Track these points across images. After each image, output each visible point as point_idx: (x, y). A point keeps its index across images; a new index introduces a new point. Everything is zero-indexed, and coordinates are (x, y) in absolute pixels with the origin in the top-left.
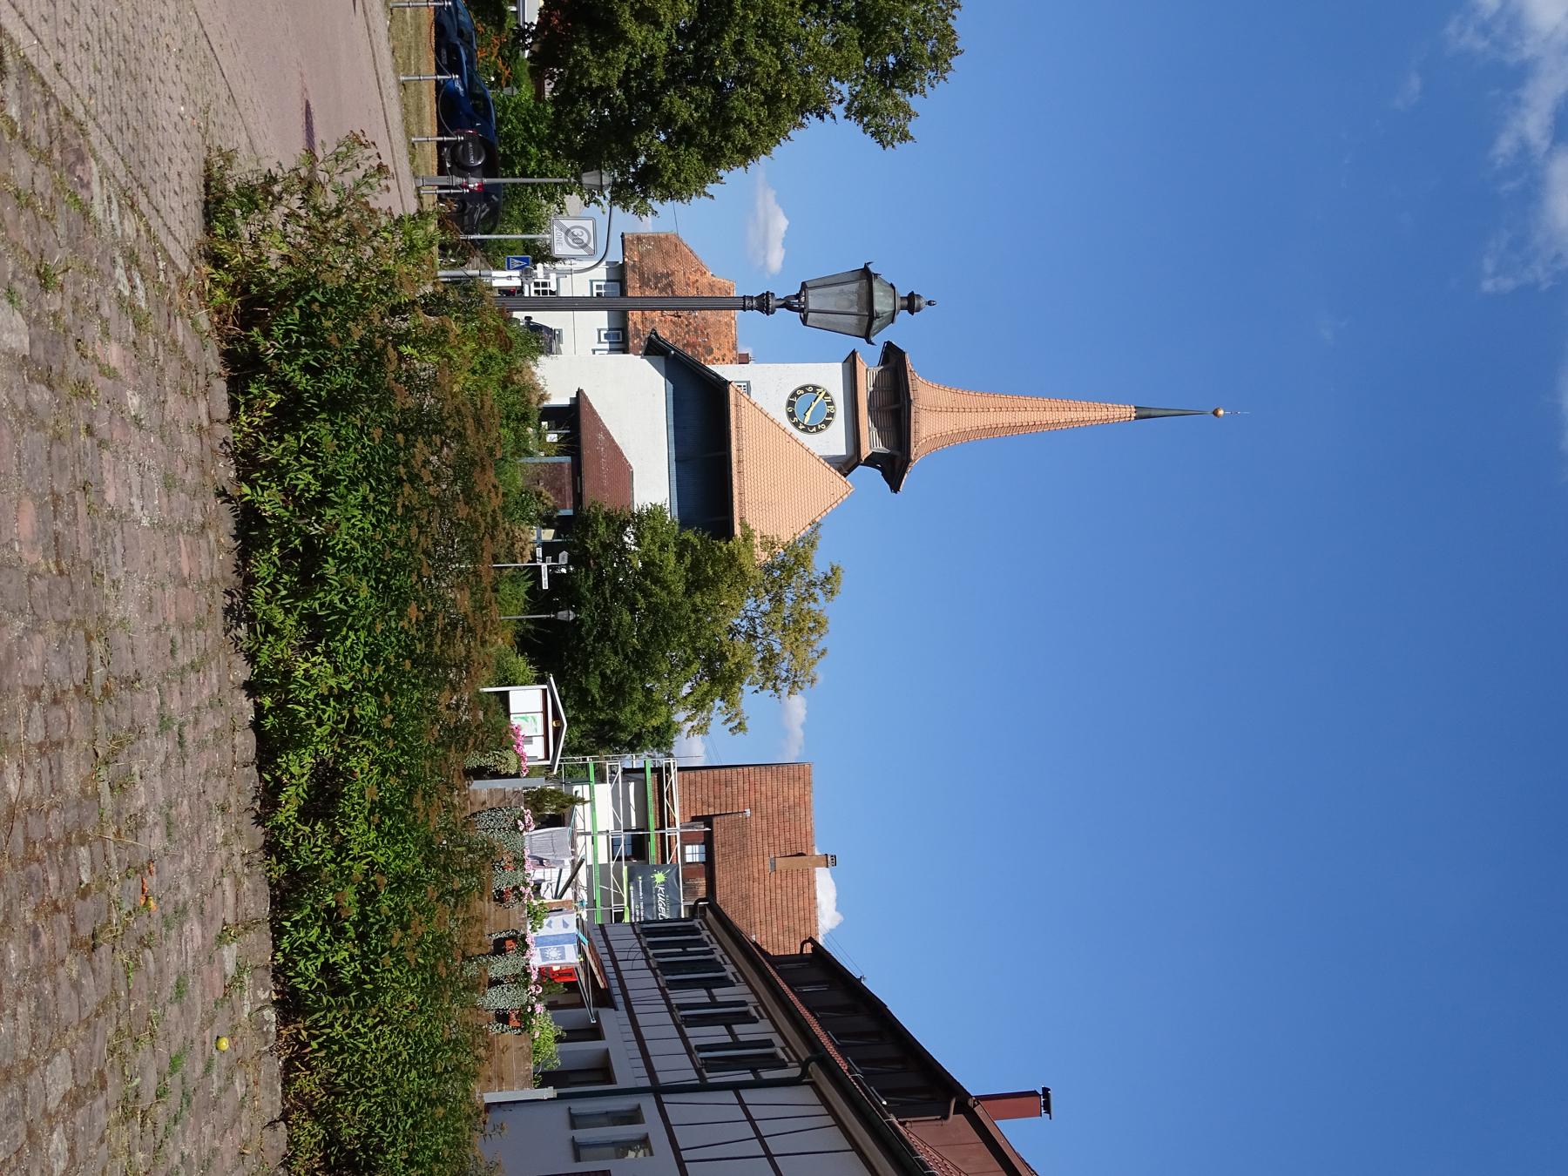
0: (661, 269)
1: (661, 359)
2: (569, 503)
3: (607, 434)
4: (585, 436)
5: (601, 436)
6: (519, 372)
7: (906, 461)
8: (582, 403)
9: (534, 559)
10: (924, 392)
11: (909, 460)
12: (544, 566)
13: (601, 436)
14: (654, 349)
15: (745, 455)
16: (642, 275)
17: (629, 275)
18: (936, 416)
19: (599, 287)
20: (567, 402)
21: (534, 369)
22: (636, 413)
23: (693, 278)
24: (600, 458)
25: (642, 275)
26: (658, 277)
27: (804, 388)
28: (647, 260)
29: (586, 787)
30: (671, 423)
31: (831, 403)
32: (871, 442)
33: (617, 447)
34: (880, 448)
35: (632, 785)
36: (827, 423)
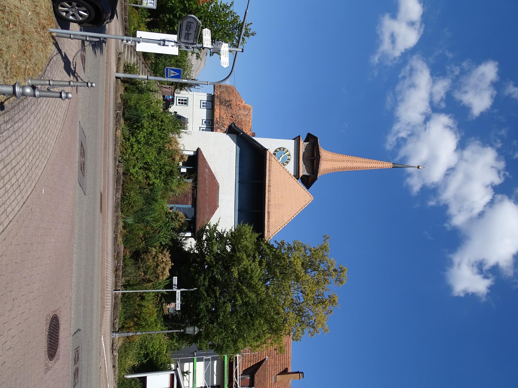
0: (227, 99)
1: (235, 136)
2: (190, 202)
3: (209, 169)
4: (200, 171)
5: (207, 170)
6: (170, 142)
7: (315, 179)
8: (200, 155)
9: (170, 285)
10: (324, 154)
11: (316, 179)
12: (178, 292)
13: (207, 170)
14: (233, 131)
15: (272, 184)
16: (220, 100)
17: (216, 99)
18: (329, 162)
19: (203, 103)
20: (192, 153)
21: (179, 140)
22: (222, 157)
23: (238, 103)
24: (205, 180)
25: (220, 100)
26: (226, 102)
27: (280, 149)
28: (222, 95)
29: (192, 364)
30: (238, 165)
31: (289, 155)
32: (303, 171)
33: (213, 175)
34: (306, 173)
35: (215, 362)
36: (287, 162)
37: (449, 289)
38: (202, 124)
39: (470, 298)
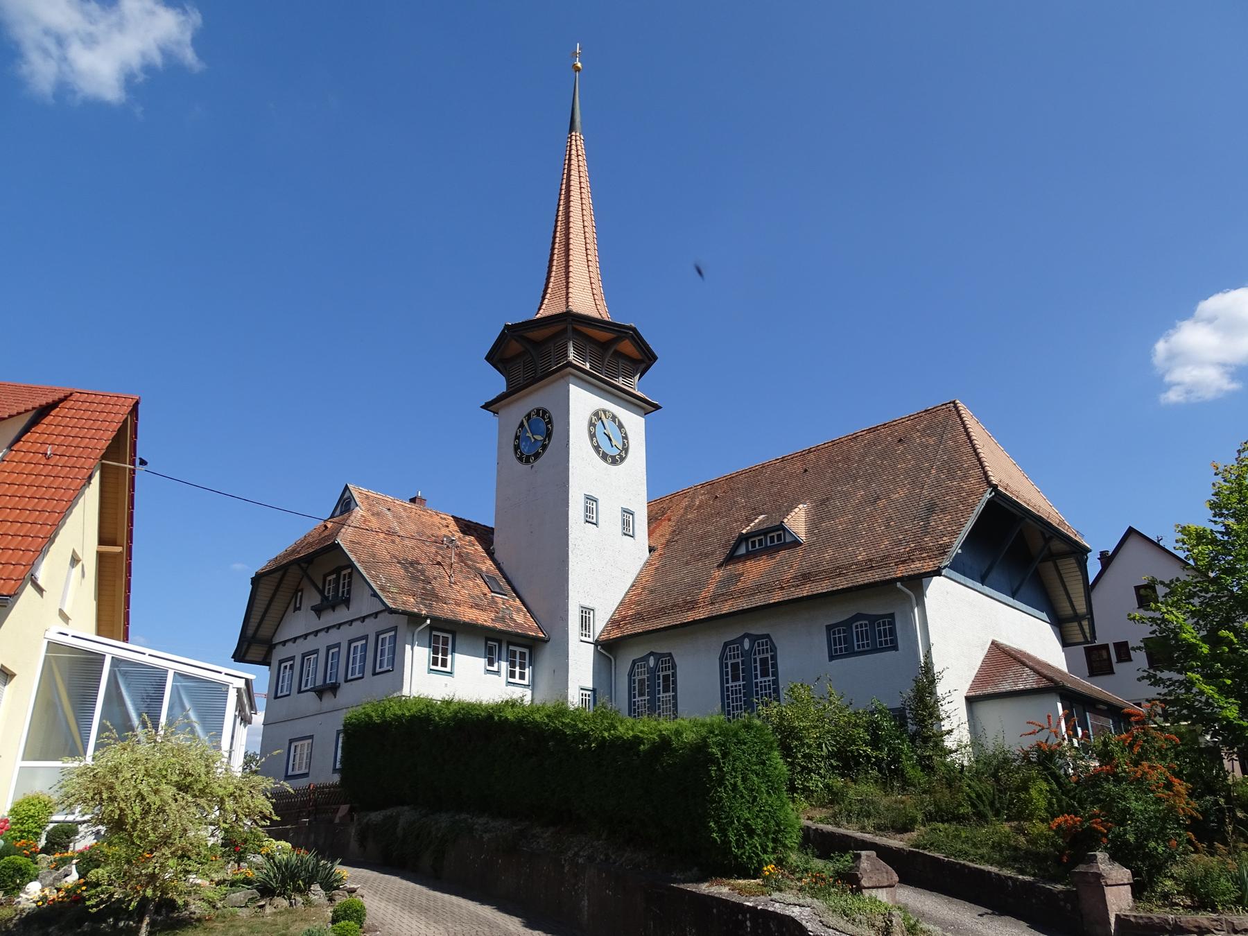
18: (585, 298)
19: (512, 675)
37: (96, 107)
38: (498, 673)
39: (153, 82)
